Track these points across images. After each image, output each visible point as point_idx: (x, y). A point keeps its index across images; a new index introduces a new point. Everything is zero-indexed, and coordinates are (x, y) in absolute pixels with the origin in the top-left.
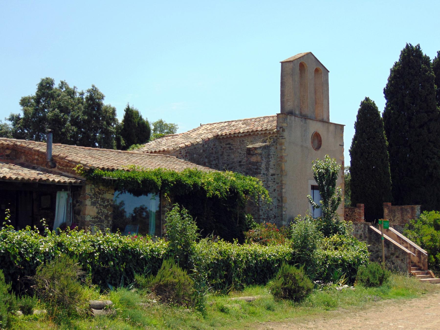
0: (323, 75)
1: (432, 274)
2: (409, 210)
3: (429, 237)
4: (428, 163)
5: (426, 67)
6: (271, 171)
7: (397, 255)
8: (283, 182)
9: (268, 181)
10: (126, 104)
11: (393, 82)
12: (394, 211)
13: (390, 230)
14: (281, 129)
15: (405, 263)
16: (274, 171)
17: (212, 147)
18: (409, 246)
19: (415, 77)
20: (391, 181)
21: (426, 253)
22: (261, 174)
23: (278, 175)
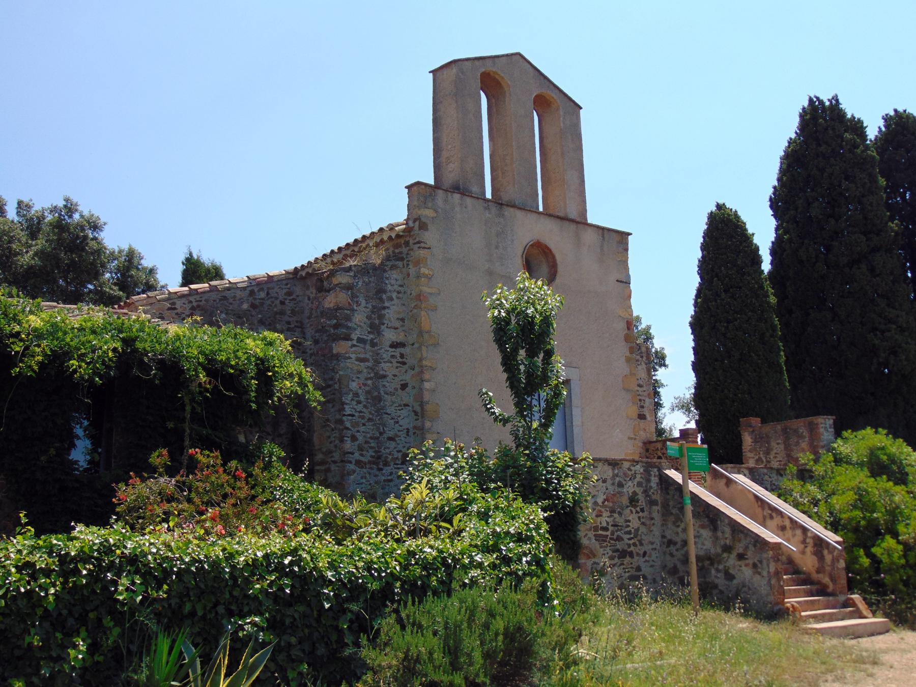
0: (562, 113)
1: (862, 606)
2: (804, 431)
3: (850, 496)
4: (877, 342)
5: (854, 138)
6: (390, 336)
7: (741, 551)
8: (424, 363)
9: (377, 362)
10: (186, 251)
11: (785, 178)
12: (767, 436)
13: (736, 482)
14: (417, 223)
15: (765, 573)
16: (402, 334)
17: (281, 298)
18: (787, 523)
19: (832, 159)
20: (787, 384)
21: (837, 542)
22: (352, 340)
23: (413, 344)
